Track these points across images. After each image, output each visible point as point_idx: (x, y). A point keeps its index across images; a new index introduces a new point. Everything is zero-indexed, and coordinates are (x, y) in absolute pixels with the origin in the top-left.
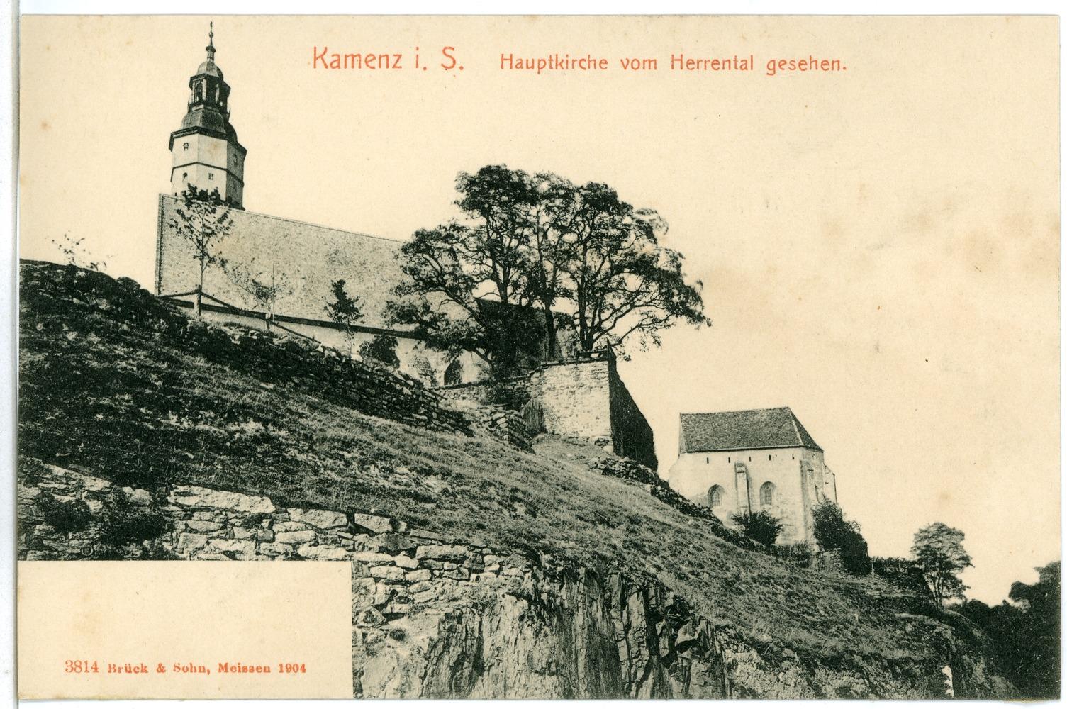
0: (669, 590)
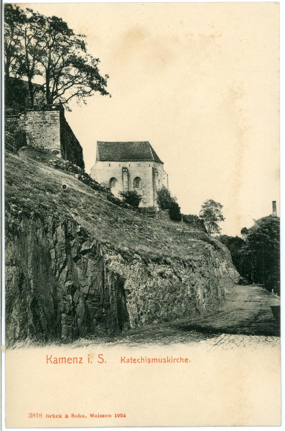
0: (79, 225)
